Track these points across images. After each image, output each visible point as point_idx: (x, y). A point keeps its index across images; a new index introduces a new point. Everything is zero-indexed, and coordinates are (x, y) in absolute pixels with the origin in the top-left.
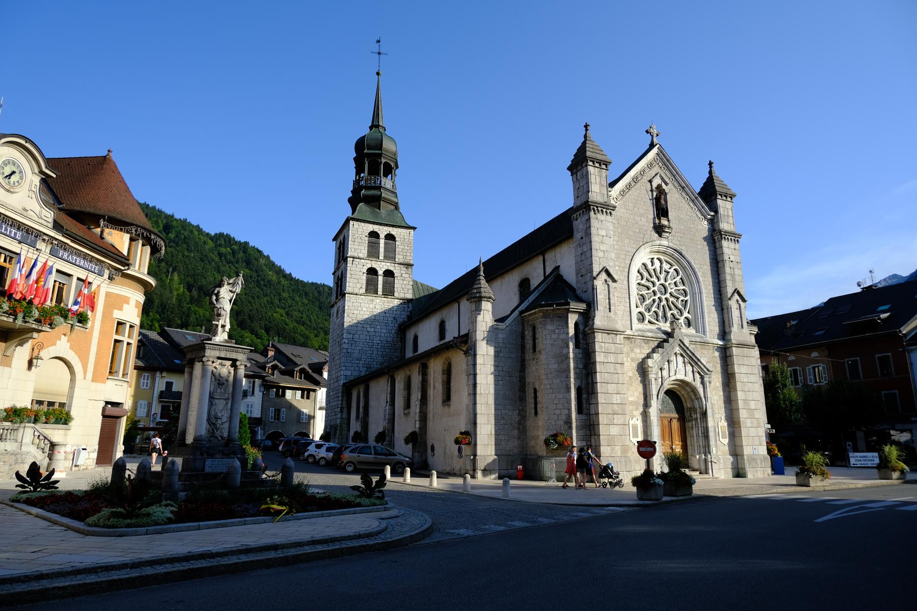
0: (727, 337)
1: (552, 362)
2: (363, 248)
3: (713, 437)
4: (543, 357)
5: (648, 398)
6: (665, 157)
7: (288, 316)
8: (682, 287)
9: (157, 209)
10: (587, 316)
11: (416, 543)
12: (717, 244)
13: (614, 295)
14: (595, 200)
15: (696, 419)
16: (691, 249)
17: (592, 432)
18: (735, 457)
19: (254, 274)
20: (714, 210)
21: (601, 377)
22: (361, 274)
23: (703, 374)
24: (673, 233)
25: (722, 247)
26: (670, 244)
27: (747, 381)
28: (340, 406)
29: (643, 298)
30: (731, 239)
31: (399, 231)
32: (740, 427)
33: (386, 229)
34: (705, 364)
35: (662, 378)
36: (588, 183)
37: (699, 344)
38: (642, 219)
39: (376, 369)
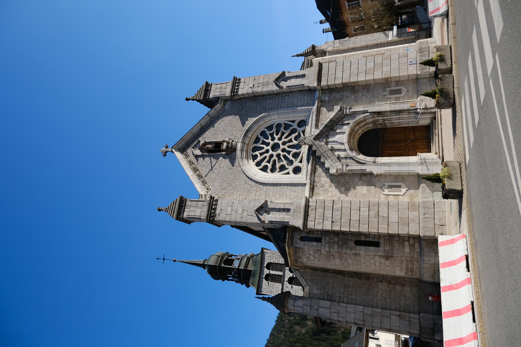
2: (276, 286)
3: (400, 105)
9: (278, 316)
14: (206, 213)
15: (384, 120)
21: (344, 226)
29: (282, 168)
38: (222, 166)
39: (371, 126)
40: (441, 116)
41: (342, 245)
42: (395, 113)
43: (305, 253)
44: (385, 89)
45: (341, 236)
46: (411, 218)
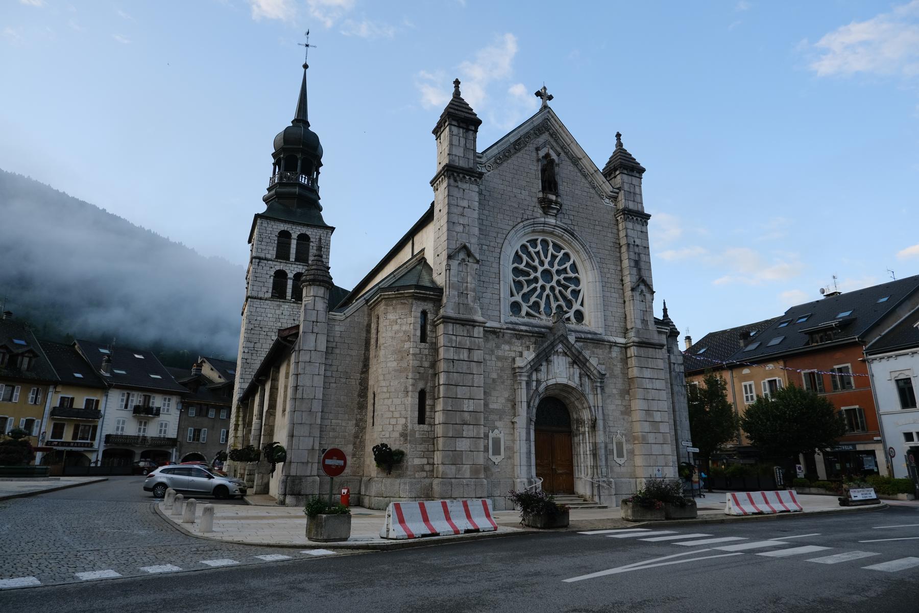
1: (391, 359)
2: (272, 249)
4: (382, 353)
6: (558, 123)
9: (152, 232)
14: (457, 164)
15: (584, 433)
17: (436, 447)
22: (268, 277)
26: (558, 222)
27: (651, 388)
29: (519, 285)
30: (637, 219)
31: (315, 231)
37: (590, 343)
40: (591, 507)
41: (419, 373)
42: (594, 448)
43: (402, 317)
44: (624, 436)
45: (431, 371)
46: (462, 467)
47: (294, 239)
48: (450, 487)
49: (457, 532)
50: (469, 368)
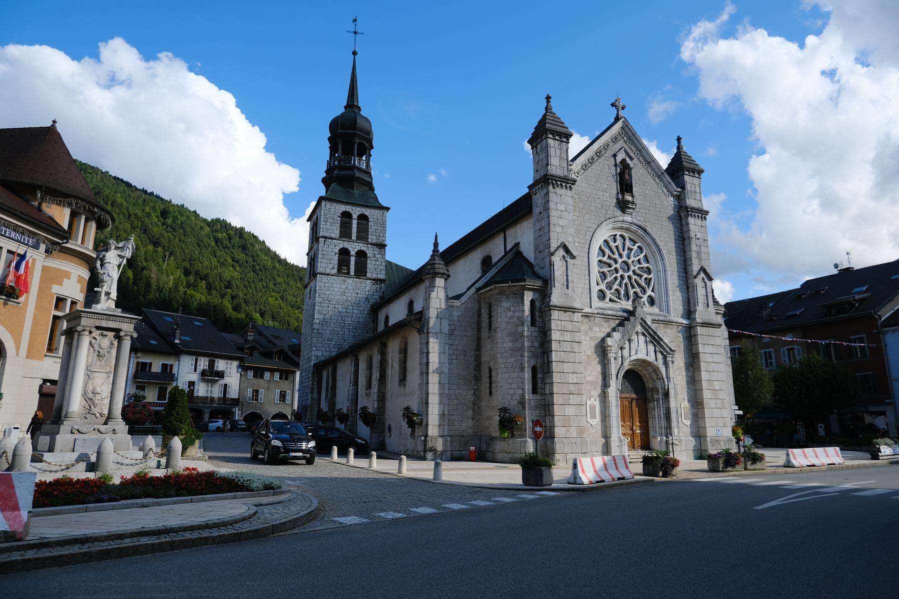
0: (693, 316)
4: (499, 334)
5: (607, 378)
7: (283, 300)
8: (646, 265)
10: (544, 292)
11: (278, 534)
12: (684, 221)
13: (572, 272)
14: (555, 173)
15: (658, 400)
16: (656, 225)
18: (698, 438)
19: (250, 260)
20: (681, 186)
21: (556, 356)
22: (333, 254)
23: (666, 353)
24: (637, 209)
25: (688, 224)
28: (310, 386)
29: (603, 276)
31: (373, 211)
32: (704, 408)
33: (359, 209)
34: (668, 343)
35: (622, 357)
36: (547, 156)
39: (650, 385)
47: (355, 219)
48: (562, 445)
49: (613, 480)
50: (572, 348)
